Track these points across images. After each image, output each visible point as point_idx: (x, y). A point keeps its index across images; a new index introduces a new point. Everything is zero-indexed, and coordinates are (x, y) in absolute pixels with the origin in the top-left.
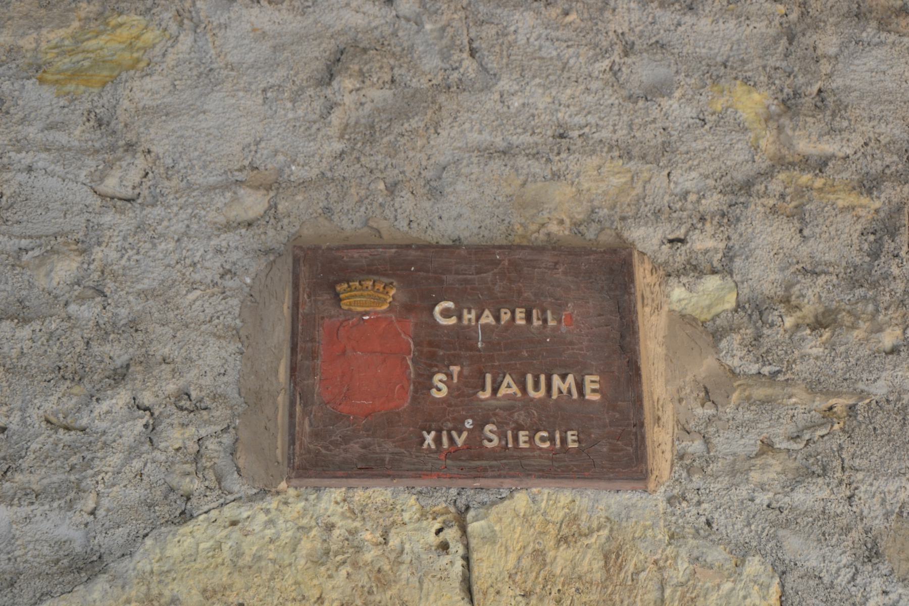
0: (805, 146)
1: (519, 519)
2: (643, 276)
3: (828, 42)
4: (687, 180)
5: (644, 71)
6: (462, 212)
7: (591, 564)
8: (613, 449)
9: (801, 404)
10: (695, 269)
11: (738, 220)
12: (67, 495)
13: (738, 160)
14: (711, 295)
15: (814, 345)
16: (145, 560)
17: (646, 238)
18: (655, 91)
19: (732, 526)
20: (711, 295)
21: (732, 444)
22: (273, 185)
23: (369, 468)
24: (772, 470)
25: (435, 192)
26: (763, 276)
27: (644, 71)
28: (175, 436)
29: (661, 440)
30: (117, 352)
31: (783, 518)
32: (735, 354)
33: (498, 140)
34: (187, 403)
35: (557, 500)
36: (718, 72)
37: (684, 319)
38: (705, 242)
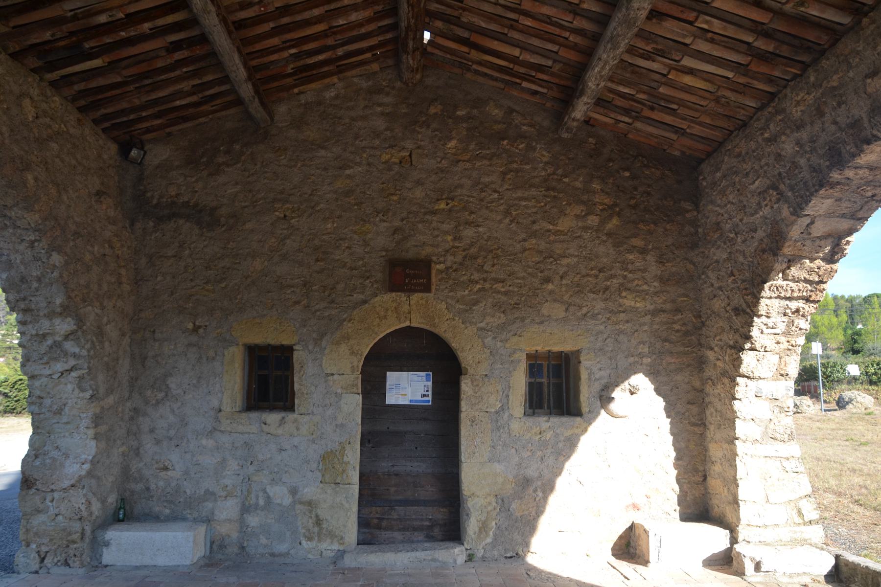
0: (456, 244)
1: (416, 297)
2: (433, 265)
3: (461, 228)
4: (440, 250)
5: (436, 233)
6: (411, 255)
7: (424, 303)
8: (427, 289)
9: (451, 282)
10: (440, 263)
11: (64, 530)
12: (363, 293)
13: (447, 247)
14: (441, 267)
15: (454, 274)
16: (372, 302)
17: (434, 258)
18: (437, 236)
19: (441, 298)
20: (441, 267)
21: (442, 287)
22: (387, 251)
23: (398, 291)
24: (447, 291)
25: (407, 252)
26: (449, 264)
27: (436, 233)
28: (375, 286)
29: (433, 287)
30: (368, 274)
31: (447, 297)
32: (444, 275)
33: (619, 15)
34: (376, 282)
35: (420, 295)
36: (447, 233)
37: (438, 270)
38: (442, 259)
